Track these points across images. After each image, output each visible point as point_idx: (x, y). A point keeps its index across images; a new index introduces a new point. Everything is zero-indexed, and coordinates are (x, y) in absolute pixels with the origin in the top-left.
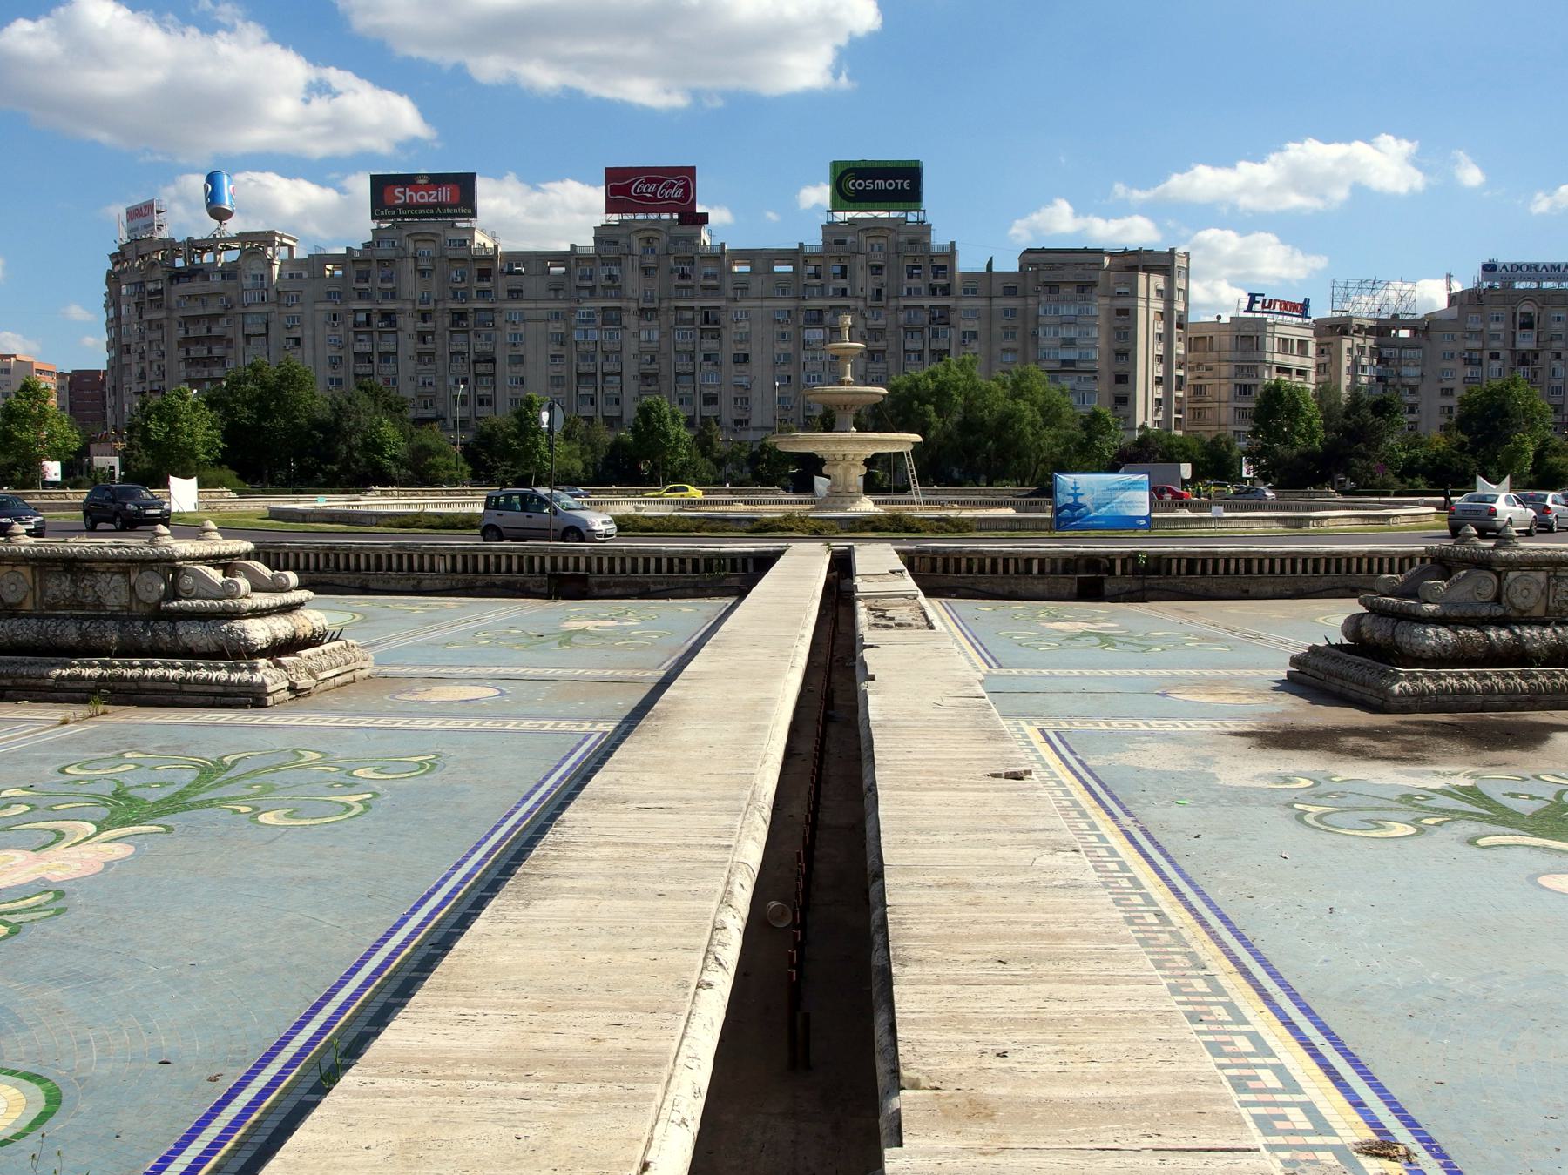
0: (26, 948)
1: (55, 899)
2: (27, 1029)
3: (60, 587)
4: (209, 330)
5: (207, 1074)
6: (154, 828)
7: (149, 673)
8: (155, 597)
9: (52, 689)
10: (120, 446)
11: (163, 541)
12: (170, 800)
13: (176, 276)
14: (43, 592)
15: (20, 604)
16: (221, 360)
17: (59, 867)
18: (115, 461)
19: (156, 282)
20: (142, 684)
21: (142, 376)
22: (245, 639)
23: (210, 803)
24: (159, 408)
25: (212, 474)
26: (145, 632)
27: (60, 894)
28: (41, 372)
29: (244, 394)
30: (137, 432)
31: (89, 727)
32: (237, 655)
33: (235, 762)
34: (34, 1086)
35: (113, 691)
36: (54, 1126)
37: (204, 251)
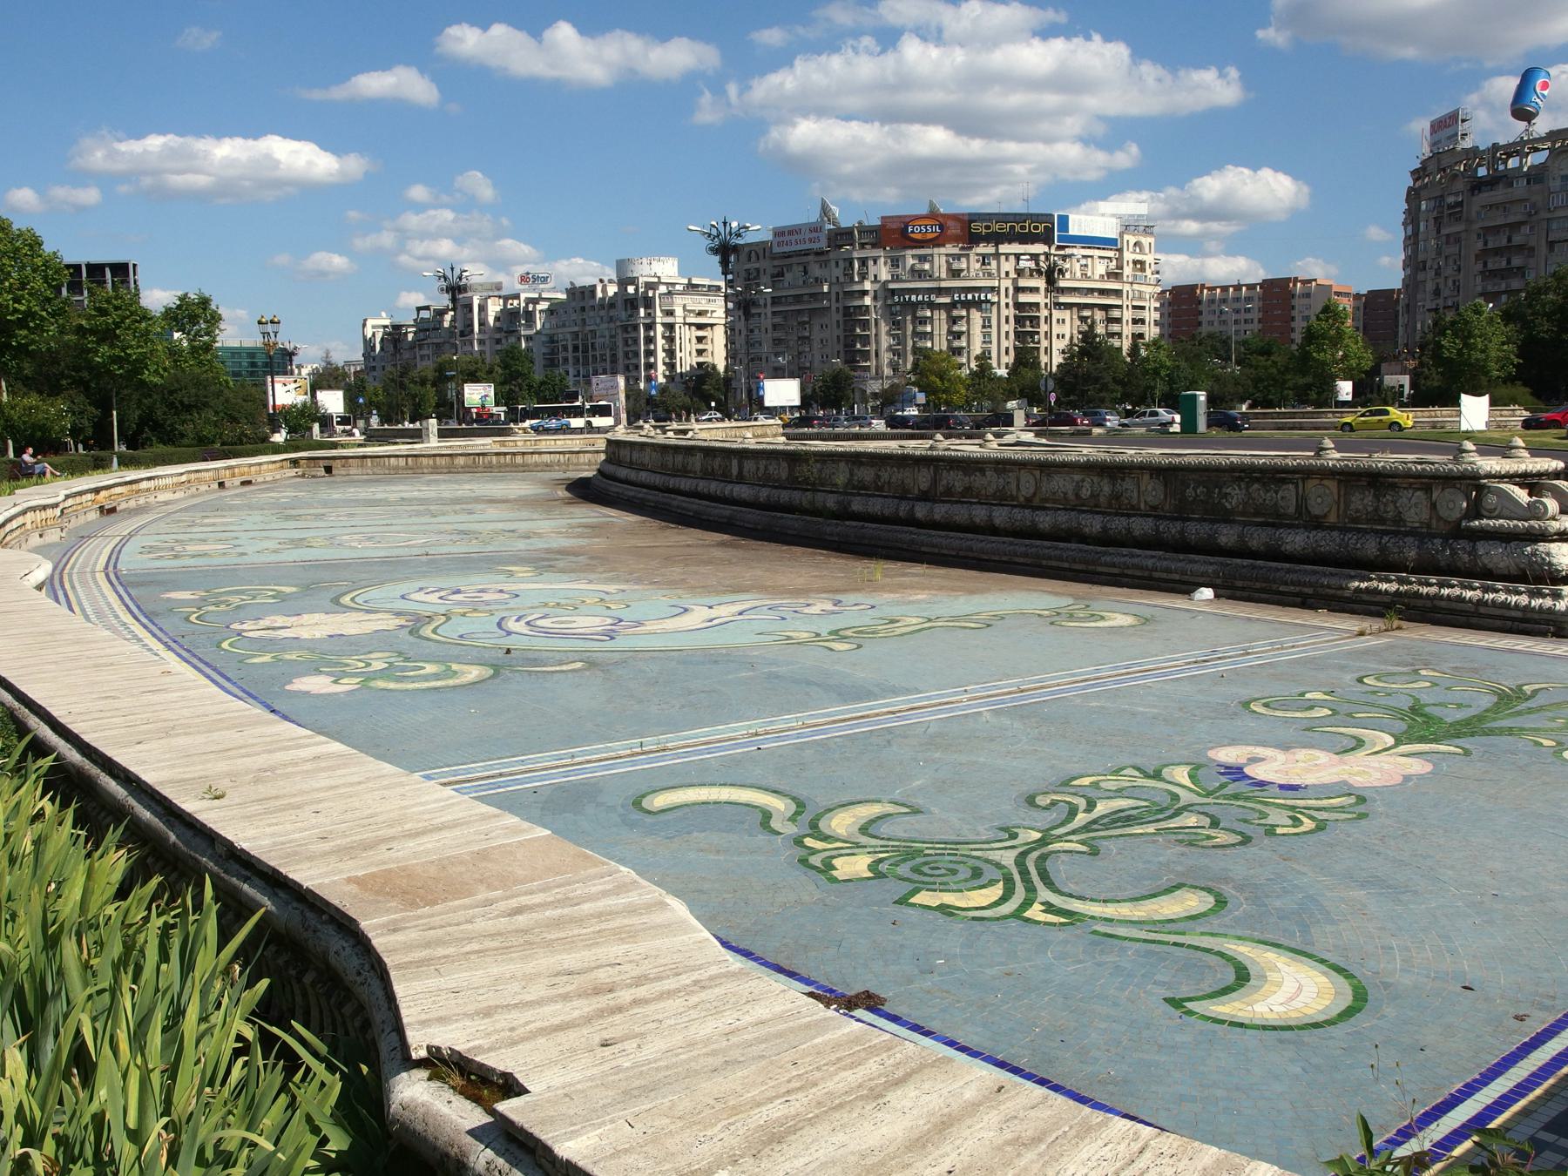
0: (1331, 845)
1: (1356, 804)
2: (1333, 922)
3: (1362, 501)
4: (1509, 240)
5: (1513, 1011)
6: (1452, 749)
7: (1445, 591)
8: (1456, 515)
9: (1349, 600)
10: (1411, 364)
11: (1468, 458)
12: (1467, 722)
13: (1478, 185)
14: (1347, 506)
15: (1325, 516)
16: (1521, 271)
17: (1359, 773)
18: (1405, 380)
19: (1456, 194)
20: (1437, 603)
21: (1437, 292)
22: (1550, 564)
23: (1510, 731)
24: (1453, 323)
25: (1503, 391)
26: (1444, 550)
27: (1361, 800)
28: (1338, 294)
29: (1544, 306)
30: (1430, 349)
31: (1383, 640)
32: (1539, 580)
33: (1535, 692)
34: (1341, 979)
35: (1408, 607)
36: (1361, 1021)
37: (1509, 155)
